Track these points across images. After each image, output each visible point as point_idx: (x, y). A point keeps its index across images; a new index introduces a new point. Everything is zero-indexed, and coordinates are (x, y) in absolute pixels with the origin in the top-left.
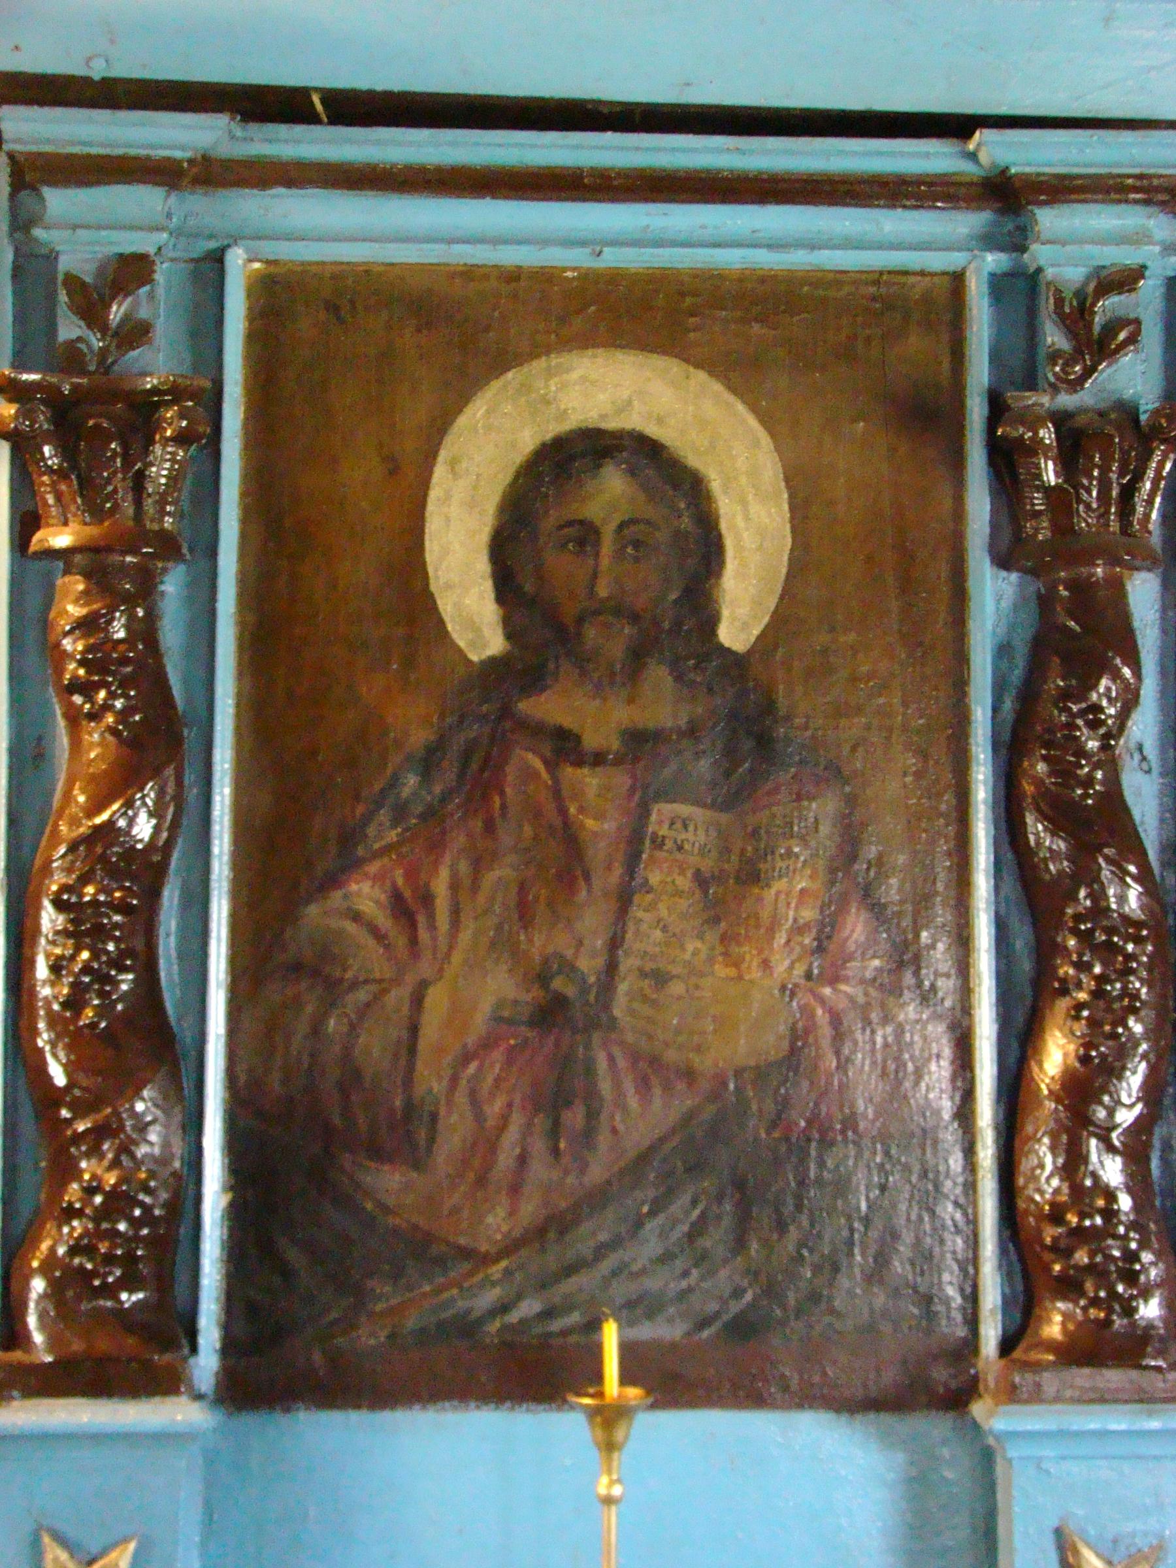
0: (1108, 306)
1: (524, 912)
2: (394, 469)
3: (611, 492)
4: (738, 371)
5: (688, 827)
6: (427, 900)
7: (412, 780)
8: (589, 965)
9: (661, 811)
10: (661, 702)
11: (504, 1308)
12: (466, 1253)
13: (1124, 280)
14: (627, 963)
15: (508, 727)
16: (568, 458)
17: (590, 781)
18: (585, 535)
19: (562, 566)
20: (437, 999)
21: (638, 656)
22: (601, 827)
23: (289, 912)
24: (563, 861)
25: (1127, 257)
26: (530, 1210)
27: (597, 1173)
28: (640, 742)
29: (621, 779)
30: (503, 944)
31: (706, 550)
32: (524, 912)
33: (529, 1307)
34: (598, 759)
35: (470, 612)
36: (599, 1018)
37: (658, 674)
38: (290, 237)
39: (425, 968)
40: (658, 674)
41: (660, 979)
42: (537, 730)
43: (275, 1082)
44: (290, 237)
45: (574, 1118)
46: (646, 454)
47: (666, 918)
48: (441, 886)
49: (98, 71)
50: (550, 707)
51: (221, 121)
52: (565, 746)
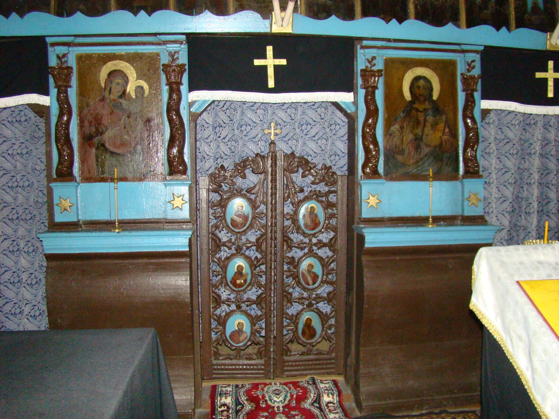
0: (473, 64)
1: (413, 128)
2: (399, 79)
3: (421, 82)
4: (434, 70)
5: (430, 118)
6: (404, 127)
7: (402, 114)
8: (420, 134)
9: (428, 117)
10: (427, 105)
11: (412, 170)
12: (408, 165)
13: (474, 61)
14: (425, 134)
15: (412, 108)
16: (417, 79)
17: (420, 114)
18: (419, 87)
19: (416, 90)
20: (405, 137)
21: (425, 100)
22: (421, 119)
23: (390, 127)
24: (418, 122)
25: (474, 59)
26: (415, 160)
27: (421, 156)
28: (425, 110)
29: (423, 114)
30: (412, 132)
31: (431, 89)
32: (413, 128)
33: (415, 171)
34: (421, 112)
35: (407, 95)
36: (421, 139)
37: (427, 103)
38: (106, 226)
39: (404, 134)
40: (427, 103)
41: (427, 135)
42: (414, 108)
43: (388, 147)
44: (106, 226)
45: (419, 150)
46: (425, 78)
47: (428, 130)
48: (405, 125)
49: (370, 37)
50: (416, 106)
51: (385, 42)
52: (417, 110)
